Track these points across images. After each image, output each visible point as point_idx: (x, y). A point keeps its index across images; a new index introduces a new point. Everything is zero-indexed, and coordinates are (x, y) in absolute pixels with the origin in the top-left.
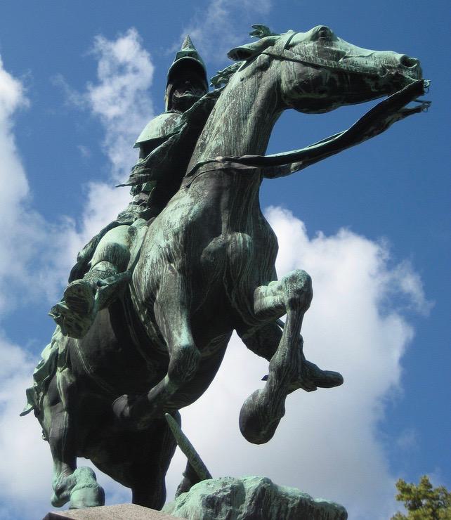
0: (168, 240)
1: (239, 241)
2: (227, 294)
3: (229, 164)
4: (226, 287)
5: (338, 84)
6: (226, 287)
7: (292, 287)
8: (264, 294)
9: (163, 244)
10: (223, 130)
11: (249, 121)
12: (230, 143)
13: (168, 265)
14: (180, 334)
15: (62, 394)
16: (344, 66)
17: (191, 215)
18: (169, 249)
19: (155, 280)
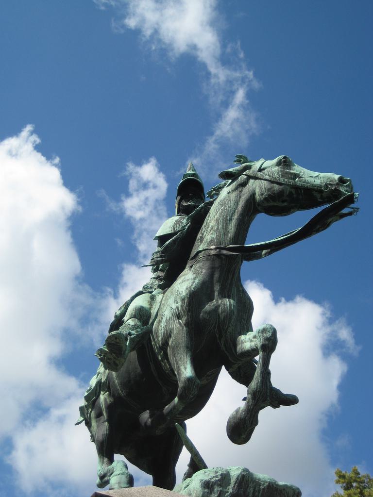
0: (177, 303)
1: (227, 304)
4: (218, 336)
6: (218, 336)
7: (263, 336)
9: (174, 306)
10: (215, 227)
11: (234, 221)
12: (220, 237)
14: (185, 368)
16: (299, 184)
17: (193, 286)
18: (178, 310)
19: (169, 331)
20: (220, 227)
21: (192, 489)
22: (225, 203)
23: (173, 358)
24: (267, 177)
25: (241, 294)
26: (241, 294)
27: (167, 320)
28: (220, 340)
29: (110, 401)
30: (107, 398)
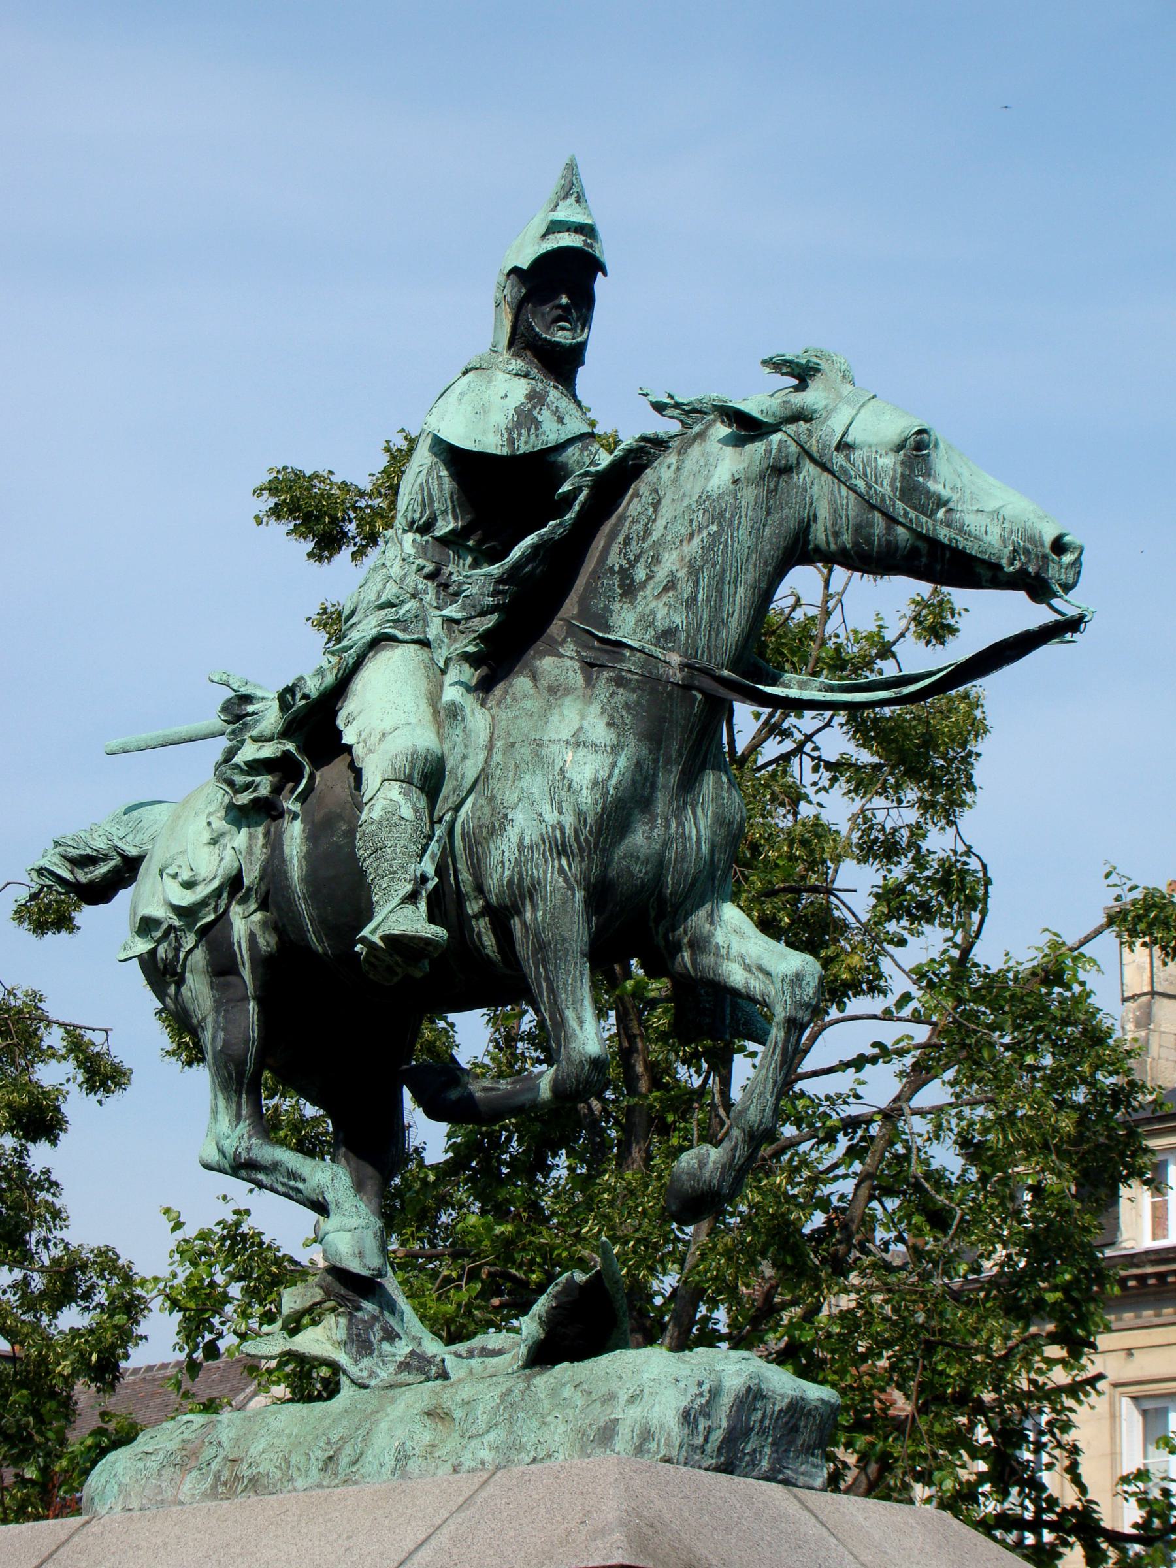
0: (561, 813)
1: (690, 838)
2: (652, 924)
3: (692, 677)
4: (653, 914)
5: (924, 560)
6: (653, 914)
7: (793, 996)
8: (723, 952)
9: (551, 817)
10: (686, 590)
11: (741, 590)
12: (699, 631)
13: (556, 863)
14: (581, 1022)
15: (247, 965)
16: (944, 534)
17: (614, 781)
18: (563, 833)
19: (527, 882)
20: (700, 595)
21: (655, 1421)
22: (722, 514)
23: (537, 968)
24: (861, 484)
25: (726, 795)
26: (726, 795)
27: (521, 844)
28: (657, 926)
29: (268, 945)
30: (258, 931)
